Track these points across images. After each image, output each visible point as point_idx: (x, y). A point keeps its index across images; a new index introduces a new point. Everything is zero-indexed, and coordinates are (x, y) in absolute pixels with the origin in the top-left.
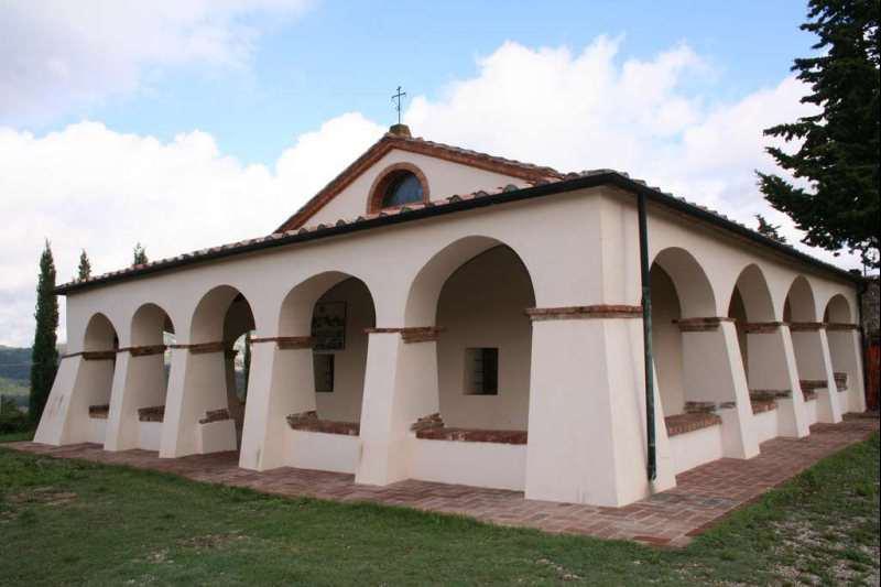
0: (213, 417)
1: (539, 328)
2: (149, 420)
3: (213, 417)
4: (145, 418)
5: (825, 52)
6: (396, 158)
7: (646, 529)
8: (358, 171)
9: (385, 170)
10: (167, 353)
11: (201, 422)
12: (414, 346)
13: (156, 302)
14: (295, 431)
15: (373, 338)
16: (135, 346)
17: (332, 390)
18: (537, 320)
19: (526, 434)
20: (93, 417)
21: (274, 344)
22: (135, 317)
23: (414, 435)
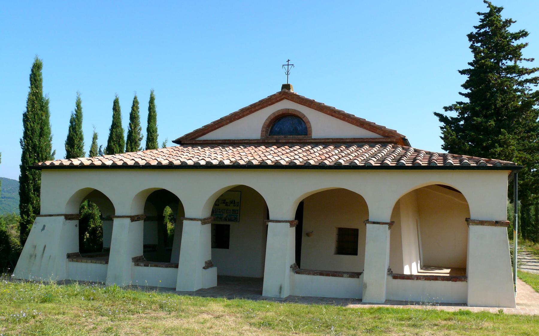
21: (63, 217)
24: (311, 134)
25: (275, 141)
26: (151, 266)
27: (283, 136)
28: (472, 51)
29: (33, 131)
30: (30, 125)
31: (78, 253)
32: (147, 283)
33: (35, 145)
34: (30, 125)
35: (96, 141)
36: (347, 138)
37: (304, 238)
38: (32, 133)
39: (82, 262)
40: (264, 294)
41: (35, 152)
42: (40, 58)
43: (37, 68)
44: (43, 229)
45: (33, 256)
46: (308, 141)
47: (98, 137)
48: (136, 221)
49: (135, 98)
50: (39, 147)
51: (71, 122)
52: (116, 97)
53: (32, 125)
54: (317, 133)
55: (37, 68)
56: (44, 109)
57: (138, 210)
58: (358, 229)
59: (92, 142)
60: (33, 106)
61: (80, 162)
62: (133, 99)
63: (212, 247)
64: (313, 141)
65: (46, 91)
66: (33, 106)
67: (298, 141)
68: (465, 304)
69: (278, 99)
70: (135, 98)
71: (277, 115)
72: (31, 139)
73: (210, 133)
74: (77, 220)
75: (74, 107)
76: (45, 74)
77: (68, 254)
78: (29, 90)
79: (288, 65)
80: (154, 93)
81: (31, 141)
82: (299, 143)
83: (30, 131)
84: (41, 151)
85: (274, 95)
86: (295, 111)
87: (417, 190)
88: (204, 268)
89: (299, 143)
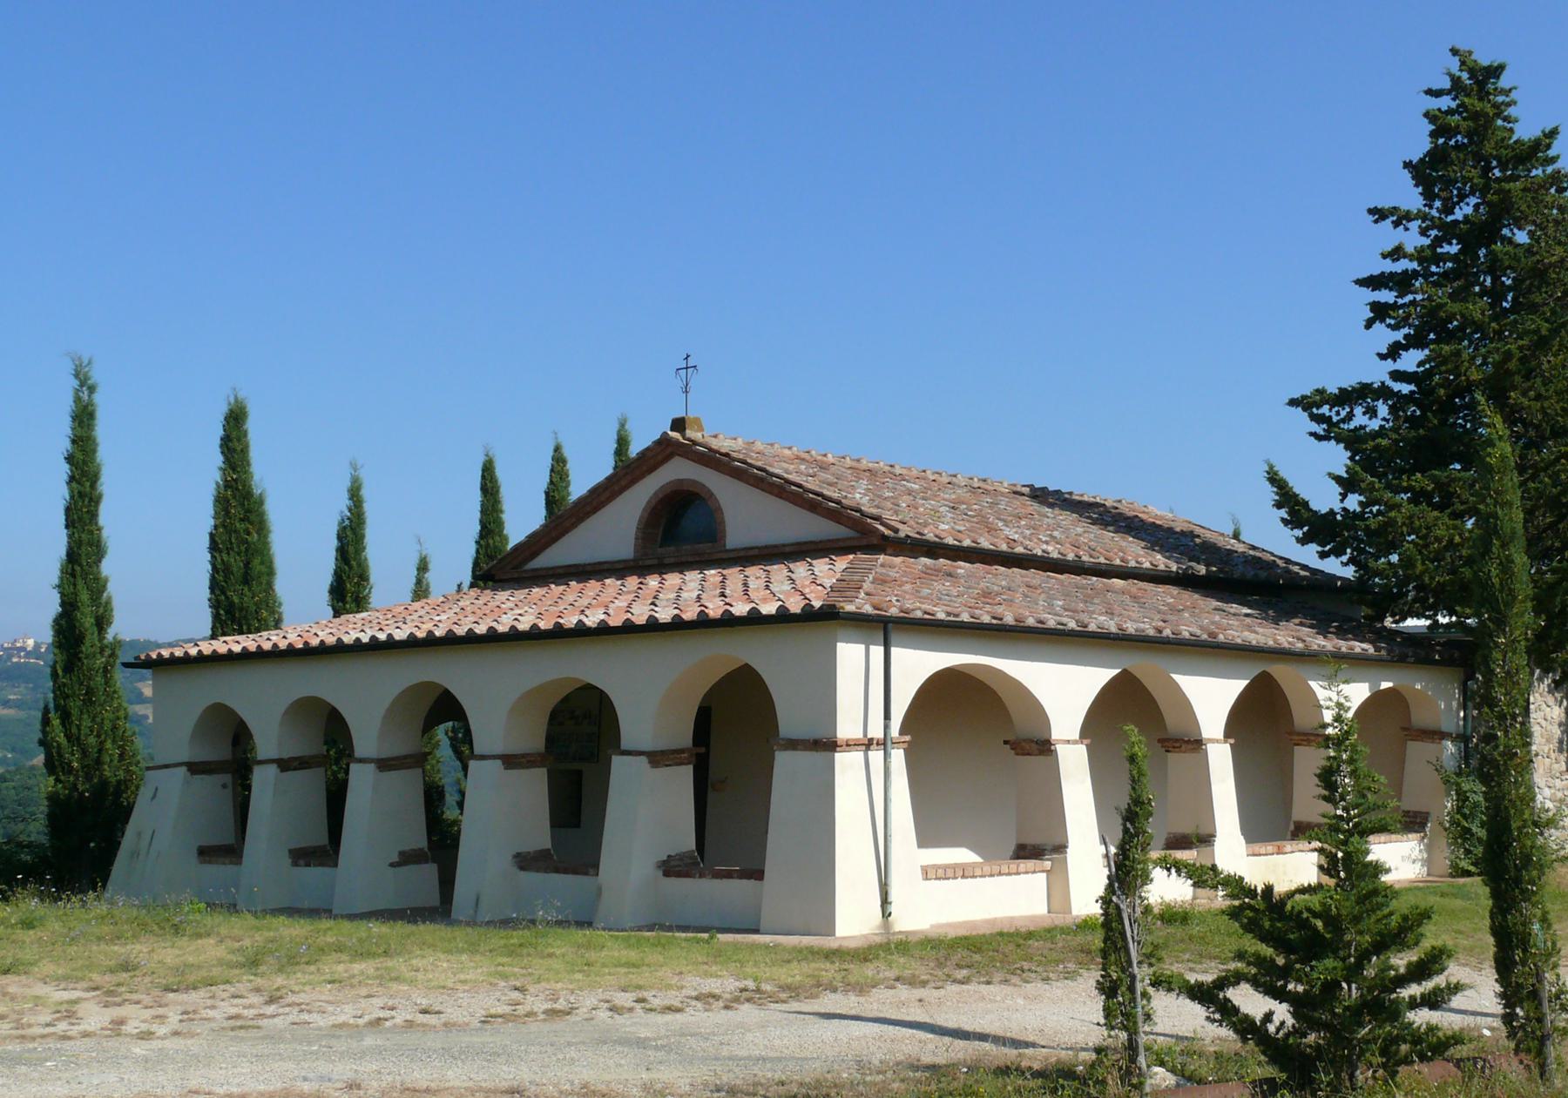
0: (408, 858)
1: (783, 760)
2: (308, 865)
3: (408, 858)
4: (302, 862)
5: (1411, 360)
6: (677, 471)
7: (817, 942)
8: (623, 483)
9: (656, 494)
10: (840, 758)
11: (392, 865)
12: (514, 773)
13: (228, 703)
14: (522, 872)
15: (617, 762)
16: (285, 755)
17: (577, 825)
18: (780, 750)
19: (763, 872)
20: (204, 862)
21: (184, 769)
22: (286, 713)
23: (661, 873)
24: (724, 537)
25: (655, 562)
26: (315, 866)
27: (672, 548)
28: (221, 469)
29: (227, 570)
30: (222, 560)
31: (325, 846)
32: (306, 905)
33: (232, 604)
34: (222, 560)
35: (426, 575)
36: (786, 542)
37: (711, 796)
38: (225, 576)
39: (217, 863)
40: (454, 915)
41: (233, 622)
42: (241, 395)
43: (235, 419)
44: (154, 797)
45: (135, 854)
46: (715, 557)
47: (431, 566)
48: (295, 769)
49: (557, 449)
50: (241, 609)
51: (340, 538)
52: (487, 455)
53: (225, 557)
54: (736, 536)
55: (235, 419)
56: (253, 517)
57: (533, 739)
58: (506, 769)
59: (414, 580)
60: (227, 513)
61: (212, 648)
62: (551, 453)
63: (553, 826)
64: (732, 555)
65: (264, 473)
66: (227, 513)
67: (698, 559)
68: (756, 931)
69: (660, 458)
70: (557, 449)
71: (661, 496)
72: (224, 593)
73: (548, 550)
74: (683, 768)
75: (342, 504)
76: (255, 428)
77: (200, 847)
78: (218, 476)
79: (687, 368)
80: (627, 427)
81: (223, 598)
82: (697, 562)
83: (221, 573)
84: (245, 618)
85: (648, 449)
86: (694, 482)
87: (449, 692)
88: (392, 865)
89: (697, 562)
